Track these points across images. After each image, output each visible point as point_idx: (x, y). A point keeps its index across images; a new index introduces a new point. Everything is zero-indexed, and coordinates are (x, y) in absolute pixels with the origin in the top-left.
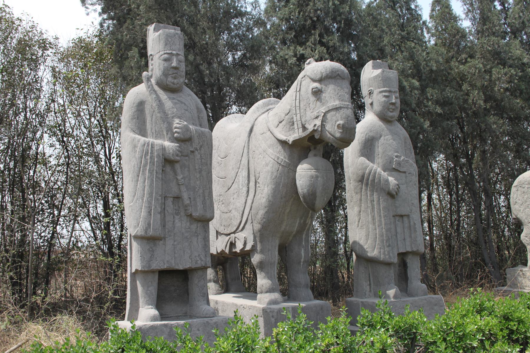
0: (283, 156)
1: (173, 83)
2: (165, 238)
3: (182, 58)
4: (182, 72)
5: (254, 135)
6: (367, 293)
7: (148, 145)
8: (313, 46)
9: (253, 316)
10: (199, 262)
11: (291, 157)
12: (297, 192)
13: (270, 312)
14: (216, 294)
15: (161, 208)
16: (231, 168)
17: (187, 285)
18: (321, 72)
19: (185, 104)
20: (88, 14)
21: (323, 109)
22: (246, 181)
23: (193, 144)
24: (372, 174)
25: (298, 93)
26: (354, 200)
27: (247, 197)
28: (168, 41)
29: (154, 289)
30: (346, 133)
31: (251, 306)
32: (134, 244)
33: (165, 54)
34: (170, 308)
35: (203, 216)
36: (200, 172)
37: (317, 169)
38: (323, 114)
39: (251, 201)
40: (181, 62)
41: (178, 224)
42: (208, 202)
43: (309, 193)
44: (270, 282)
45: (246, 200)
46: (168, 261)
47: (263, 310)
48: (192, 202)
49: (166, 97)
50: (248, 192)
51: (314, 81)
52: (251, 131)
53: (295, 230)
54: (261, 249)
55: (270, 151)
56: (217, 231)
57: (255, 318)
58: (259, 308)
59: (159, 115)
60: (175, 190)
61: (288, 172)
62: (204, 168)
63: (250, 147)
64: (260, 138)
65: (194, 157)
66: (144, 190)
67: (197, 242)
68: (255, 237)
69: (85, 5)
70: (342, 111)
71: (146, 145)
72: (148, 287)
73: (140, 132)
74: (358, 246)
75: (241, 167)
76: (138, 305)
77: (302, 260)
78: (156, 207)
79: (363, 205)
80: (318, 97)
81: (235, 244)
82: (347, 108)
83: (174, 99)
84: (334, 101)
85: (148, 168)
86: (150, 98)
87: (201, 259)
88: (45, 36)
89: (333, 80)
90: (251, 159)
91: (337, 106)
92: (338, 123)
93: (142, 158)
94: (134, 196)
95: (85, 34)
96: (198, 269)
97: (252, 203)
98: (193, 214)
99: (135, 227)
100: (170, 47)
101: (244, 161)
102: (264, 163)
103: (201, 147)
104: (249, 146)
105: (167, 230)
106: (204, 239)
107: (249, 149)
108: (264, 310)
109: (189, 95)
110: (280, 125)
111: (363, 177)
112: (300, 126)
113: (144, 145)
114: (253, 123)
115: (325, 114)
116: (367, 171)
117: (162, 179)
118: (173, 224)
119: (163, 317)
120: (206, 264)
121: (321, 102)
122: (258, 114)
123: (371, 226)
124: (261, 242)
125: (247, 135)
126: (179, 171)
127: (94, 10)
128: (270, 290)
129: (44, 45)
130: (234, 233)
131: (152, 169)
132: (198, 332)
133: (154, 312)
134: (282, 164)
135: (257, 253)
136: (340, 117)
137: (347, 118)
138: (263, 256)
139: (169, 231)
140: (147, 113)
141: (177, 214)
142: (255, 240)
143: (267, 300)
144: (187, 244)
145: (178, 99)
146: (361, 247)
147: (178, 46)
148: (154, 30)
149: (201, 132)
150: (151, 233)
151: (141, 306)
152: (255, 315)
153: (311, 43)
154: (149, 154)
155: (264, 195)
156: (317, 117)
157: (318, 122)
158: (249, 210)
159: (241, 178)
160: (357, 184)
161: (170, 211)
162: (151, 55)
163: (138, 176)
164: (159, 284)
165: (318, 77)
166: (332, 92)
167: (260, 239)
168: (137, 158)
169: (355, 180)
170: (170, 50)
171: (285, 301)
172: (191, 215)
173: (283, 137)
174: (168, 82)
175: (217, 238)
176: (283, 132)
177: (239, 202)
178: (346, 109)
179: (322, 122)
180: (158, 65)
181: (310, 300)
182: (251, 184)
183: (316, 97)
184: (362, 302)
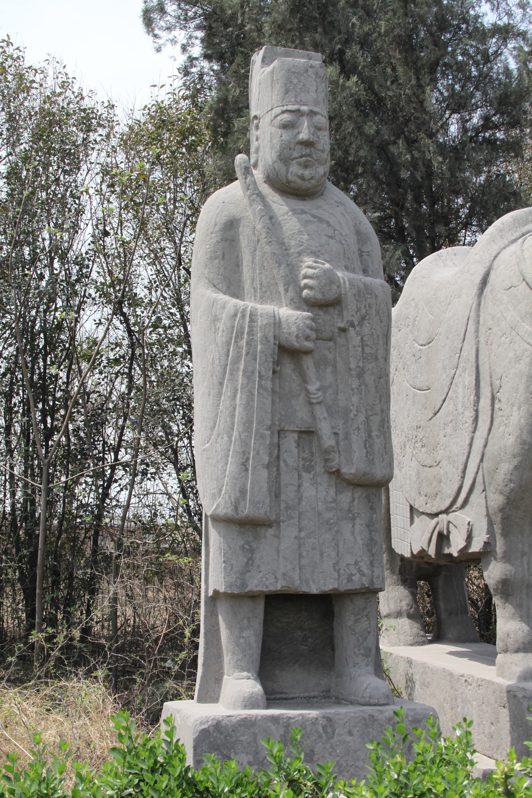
1: (302, 178)
2: (278, 523)
3: (323, 120)
4: (323, 151)
5: (492, 291)
7: (243, 316)
9: (460, 720)
10: (356, 578)
13: (524, 697)
14: (412, 645)
15: (270, 454)
16: (440, 365)
17: (332, 629)
19: (329, 224)
20: (158, 50)
22: (472, 397)
23: (345, 313)
27: (474, 432)
28: (291, 84)
29: (253, 635)
32: (213, 534)
33: (283, 112)
34: (290, 678)
35: (365, 474)
36: (360, 376)
39: (483, 442)
40: (319, 129)
41: (309, 491)
42: (378, 443)
44: (525, 628)
45: (472, 438)
46: (284, 575)
47: (508, 692)
48: (342, 443)
49: (285, 208)
50: (476, 420)
52: (484, 282)
54: (505, 552)
56: (412, 508)
57: (464, 725)
59: (268, 248)
60: (302, 415)
62: (370, 366)
63: (481, 319)
64: (505, 297)
65: (347, 340)
66: (233, 416)
67: (353, 533)
68: (491, 524)
69: (153, 30)
71: (239, 315)
72: (241, 630)
73: (228, 287)
75: (461, 365)
76: (221, 667)
78: (258, 454)
81: (447, 537)
83: (303, 212)
85: (242, 367)
86: (249, 213)
87: (360, 571)
88: (87, 103)
90: (482, 346)
93: (229, 345)
94: (212, 429)
95: (170, 96)
96: (358, 594)
97: (485, 446)
98: (344, 470)
99: (214, 497)
100: (296, 96)
101: (469, 351)
102: (511, 354)
103: (363, 319)
104: (478, 316)
105: (283, 505)
106: (368, 526)
107: (478, 323)
109: (340, 204)
113: (235, 315)
114: (488, 265)
117: (273, 391)
118: (299, 491)
119: (272, 698)
120: (372, 582)
122: (501, 243)
124: (505, 534)
125: (474, 291)
126: (311, 372)
127: (172, 41)
129: (88, 121)
130: (446, 511)
131: (250, 369)
132: (348, 738)
133: (252, 686)
135: (496, 559)
138: (508, 567)
139: (288, 508)
140: (243, 245)
141: (308, 469)
142: (490, 530)
144: (328, 537)
145: (314, 212)
147: (313, 94)
148: (263, 61)
149: (362, 286)
150: (247, 510)
151: (226, 671)
152: (465, 720)
154: (245, 336)
155: (510, 429)
158: (478, 461)
159: (460, 390)
161: (291, 462)
162: (256, 117)
163: (221, 384)
164: (266, 622)
167: (503, 529)
168: (220, 343)
170: (296, 102)
172: (338, 471)
174: (290, 177)
175: (412, 522)
180: (268, 138)
182: (482, 403)
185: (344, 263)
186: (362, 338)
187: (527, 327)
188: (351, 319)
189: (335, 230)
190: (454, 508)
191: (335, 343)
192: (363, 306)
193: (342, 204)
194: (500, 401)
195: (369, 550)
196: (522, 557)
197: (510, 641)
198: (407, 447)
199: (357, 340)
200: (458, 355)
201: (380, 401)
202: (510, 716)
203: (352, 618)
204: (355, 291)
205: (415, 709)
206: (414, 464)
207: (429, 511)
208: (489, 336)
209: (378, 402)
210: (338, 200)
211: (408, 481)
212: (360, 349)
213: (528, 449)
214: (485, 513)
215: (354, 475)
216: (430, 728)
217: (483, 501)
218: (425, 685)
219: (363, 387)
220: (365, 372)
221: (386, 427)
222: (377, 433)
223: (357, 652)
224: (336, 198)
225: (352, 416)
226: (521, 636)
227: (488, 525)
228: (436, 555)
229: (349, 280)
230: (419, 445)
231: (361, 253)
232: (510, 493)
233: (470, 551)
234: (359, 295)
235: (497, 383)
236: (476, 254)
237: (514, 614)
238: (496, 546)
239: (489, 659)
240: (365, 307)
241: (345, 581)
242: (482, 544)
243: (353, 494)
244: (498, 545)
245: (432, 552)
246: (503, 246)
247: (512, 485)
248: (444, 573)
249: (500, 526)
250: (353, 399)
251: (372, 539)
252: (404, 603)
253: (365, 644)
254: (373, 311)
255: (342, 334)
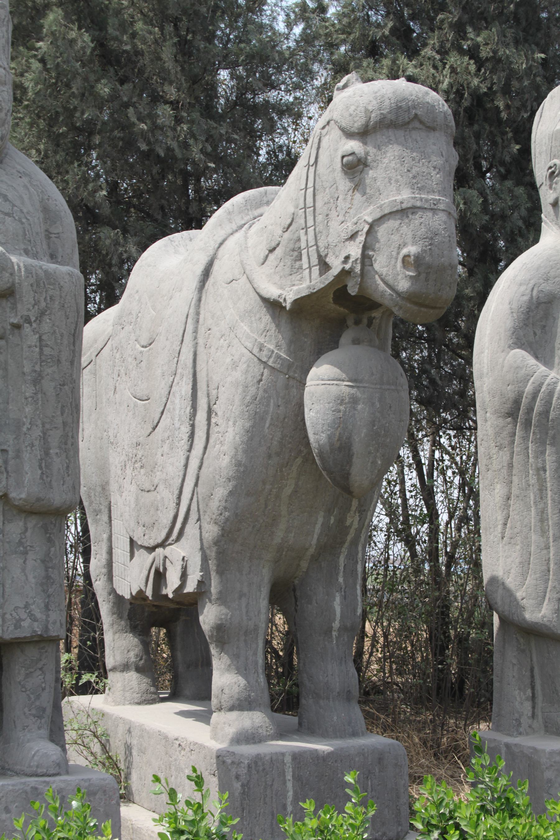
0: (274, 342)
6: (525, 721)
8: (438, 57)
10: (25, 624)
11: (294, 345)
12: (308, 444)
13: (233, 763)
14: (139, 704)
16: (159, 372)
18: (366, 110)
21: (368, 215)
22: (189, 408)
23: (19, 306)
24: (541, 395)
25: (312, 169)
26: (495, 465)
27: (189, 451)
30: (427, 280)
31: (196, 744)
35: (38, 500)
36: (37, 380)
37: (355, 380)
38: (367, 227)
42: (58, 463)
43: (331, 445)
44: (242, 681)
45: (188, 458)
47: (218, 757)
48: (11, 462)
50: (192, 436)
51: (349, 134)
52: (207, 273)
53: (314, 542)
54: (220, 592)
55: (244, 328)
56: (132, 541)
58: (210, 750)
61: (287, 387)
62: (49, 371)
63: (201, 317)
67: (23, 570)
68: (205, 559)
70: (417, 219)
74: (500, 591)
75: (179, 371)
77: (336, 625)
79: (515, 479)
80: (357, 179)
82: (434, 210)
84: (398, 190)
89: (400, 133)
90: (200, 349)
91: (404, 206)
92: (405, 251)
96: (30, 642)
97: (200, 468)
98: (13, 495)
102: (228, 360)
103: (42, 313)
104: (198, 314)
106: (43, 561)
107: (198, 321)
108: (220, 757)
109: (22, 174)
110: (272, 257)
111: (517, 402)
112: (315, 260)
114: (212, 253)
115: (372, 227)
116: (529, 388)
120: (46, 629)
121: (364, 194)
122: (228, 228)
123: (534, 537)
124: (220, 572)
128: (242, 704)
130: (162, 545)
134: (270, 363)
136: (410, 235)
137: (431, 238)
138: (224, 610)
142: (205, 567)
143: (231, 731)
146: (509, 593)
149: (42, 274)
153: (433, 48)
155: (225, 448)
156: (353, 237)
157: (355, 250)
158: (192, 485)
159: (177, 401)
160: (501, 422)
165: (358, 124)
166: (393, 164)
167: (218, 566)
169: (496, 412)
171: (282, 734)
173: (272, 291)
175: (132, 556)
176: (277, 278)
177: (172, 464)
178: (430, 214)
179: (365, 248)
181: (354, 734)
183: (351, 180)
184: (507, 746)
185: (23, 246)
186: (40, 337)
187: (245, 328)
188: (26, 313)
189: (14, 205)
190: (170, 541)
191: (7, 342)
192: (42, 299)
193: (26, 175)
194: (216, 414)
195: (44, 591)
196: (240, 598)
197: (225, 697)
198: (127, 467)
199: (33, 339)
200: (176, 359)
201: (62, 414)
202: (220, 785)
203: (23, 671)
204: (32, 281)
205: (90, 780)
206: (133, 488)
207: (146, 544)
208: (208, 338)
209: (59, 413)
210: (22, 170)
211: (127, 508)
212: (37, 350)
213: (244, 471)
214: (199, 547)
215: (25, 500)
216: (52, 802)
217: (198, 532)
218: (142, 751)
219: (39, 396)
220: (43, 378)
221: (69, 443)
222: (58, 451)
223: (28, 713)
224: (19, 167)
225: (25, 429)
226: (237, 691)
227: (202, 560)
228: (153, 596)
229: (25, 266)
230: (138, 465)
231: (48, 235)
232: (225, 523)
233: (185, 591)
234: (38, 285)
235: (214, 393)
236: (201, 240)
237: (229, 666)
238: (210, 585)
239: (204, 717)
240: (45, 299)
241: (11, 628)
242: (196, 583)
243: (25, 524)
244: (213, 585)
245: (149, 593)
246: (230, 231)
247: (227, 514)
248: (183, 618)
249: (215, 562)
250: (27, 410)
251: (48, 577)
252: (132, 654)
253: (38, 703)
254: (56, 305)
255: (16, 331)
